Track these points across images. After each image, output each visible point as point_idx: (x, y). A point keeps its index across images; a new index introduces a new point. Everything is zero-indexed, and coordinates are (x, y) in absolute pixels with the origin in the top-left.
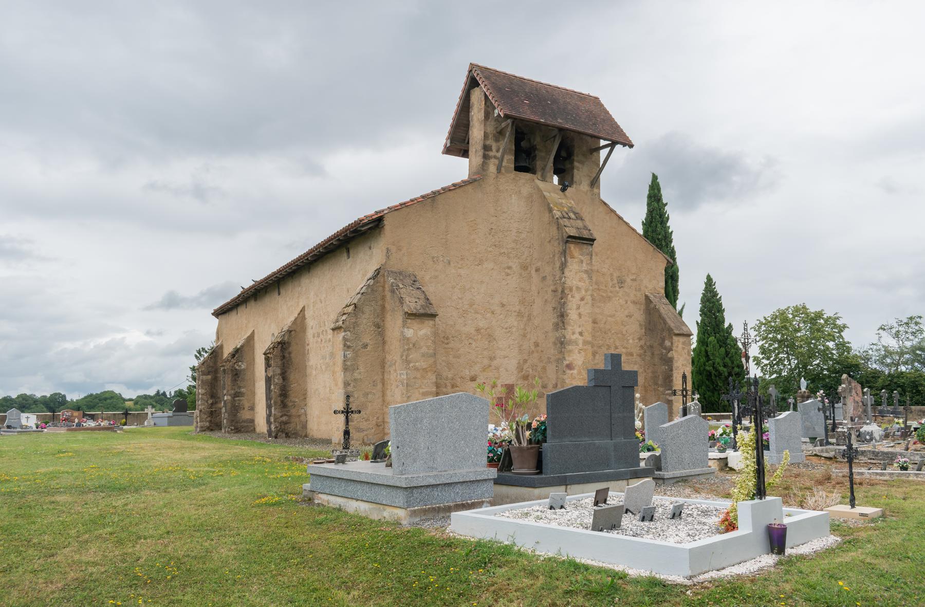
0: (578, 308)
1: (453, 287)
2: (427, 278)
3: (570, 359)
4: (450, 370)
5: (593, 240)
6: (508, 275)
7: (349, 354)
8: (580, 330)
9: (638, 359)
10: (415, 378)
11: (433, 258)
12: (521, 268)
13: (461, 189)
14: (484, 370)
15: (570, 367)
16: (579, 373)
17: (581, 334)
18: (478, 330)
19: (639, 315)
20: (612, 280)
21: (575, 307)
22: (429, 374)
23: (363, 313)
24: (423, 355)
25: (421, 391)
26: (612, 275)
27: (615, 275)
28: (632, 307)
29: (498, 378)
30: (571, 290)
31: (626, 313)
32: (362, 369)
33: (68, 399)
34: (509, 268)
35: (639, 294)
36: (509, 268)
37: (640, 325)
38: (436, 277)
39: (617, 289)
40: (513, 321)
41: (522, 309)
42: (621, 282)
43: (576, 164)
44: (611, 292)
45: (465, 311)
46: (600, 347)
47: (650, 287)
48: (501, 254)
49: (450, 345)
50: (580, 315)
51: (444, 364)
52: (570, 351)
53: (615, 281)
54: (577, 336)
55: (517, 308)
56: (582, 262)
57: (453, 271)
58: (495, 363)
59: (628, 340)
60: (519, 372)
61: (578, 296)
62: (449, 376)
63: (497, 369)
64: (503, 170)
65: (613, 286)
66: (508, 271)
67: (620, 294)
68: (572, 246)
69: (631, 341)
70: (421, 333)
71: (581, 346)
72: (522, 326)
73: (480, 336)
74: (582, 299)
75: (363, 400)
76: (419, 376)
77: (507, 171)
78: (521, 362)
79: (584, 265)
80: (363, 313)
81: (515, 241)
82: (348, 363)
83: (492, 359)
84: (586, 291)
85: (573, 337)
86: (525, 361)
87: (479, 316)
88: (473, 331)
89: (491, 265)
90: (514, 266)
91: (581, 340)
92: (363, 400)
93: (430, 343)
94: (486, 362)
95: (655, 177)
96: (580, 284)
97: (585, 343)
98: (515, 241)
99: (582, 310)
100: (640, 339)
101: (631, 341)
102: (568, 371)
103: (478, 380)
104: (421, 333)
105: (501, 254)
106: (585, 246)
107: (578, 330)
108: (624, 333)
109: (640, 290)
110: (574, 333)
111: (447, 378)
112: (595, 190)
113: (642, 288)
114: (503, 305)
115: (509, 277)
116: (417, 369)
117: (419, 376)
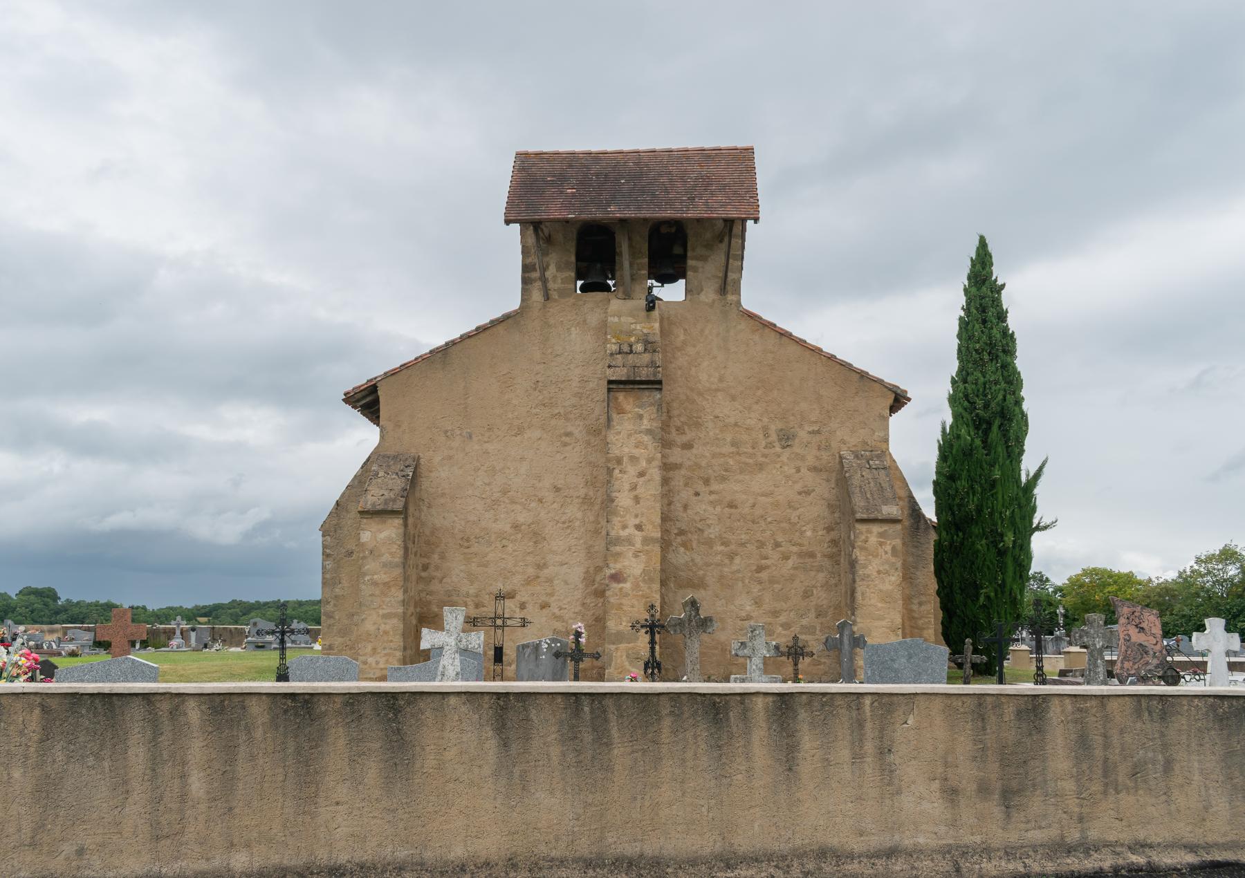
0: (634, 487)
1: (477, 470)
2: (437, 459)
3: (618, 566)
4: (472, 583)
5: (660, 382)
6: (565, 445)
7: (330, 564)
8: (637, 521)
9: (827, 563)
10: (371, 595)
11: (446, 432)
12: (588, 433)
13: (488, 332)
14: (528, 582)
15: (617, 578)
16: (636, 586)
17: (639, 527)
18: (516, 527)
19: (824, 489)
20: (766, 435)
21: (627, 486)
22: (393, 590)
23: (348, 512)
24: (384, 565)
25: (381, 612)
26: (765, 430)
27: (773, 427)
28: (809, 478)
29: (552, 595)
30: (619, 461)
31: (798, 487)
32: (345, 583)
33: (150, 608)
34: (568, 434)
35: (825, 455)
36: (568, 434)
37: (830, 506)
38: (450, 458)
39: (778, 449)
40: (573, 511)
41: (591, 493)
42: (786, 438)
43: (690, 263)
44: (765, 456)
45: (496, 502)
46: (743, 545)
47: (853, 441)
48: (553, 416)
49: (472, 550)
50: (637, 499)
51: (462, 575)
52: (619, 554)
53: (774, 437)
54: (631, 530)
55: (582, 492)
56: (641, 417)
57: (476, 447)
58: (546, 572)
59: (802, 533)
60: (587, 586)
61: (632, 471)
62: (471, 592)
63: (550, 580)
64: (555, 295)
65: (770, 445)
66: (567, 439)
67: (784, 458)
68: (621, 396)
69: (809, 533)
70: (383, 535)
71: (638, 545)
72: (592, 518)
73: (520, 536)
74: (641, 474)
75: (346, 622)
76: (377, 592)
77: (563, 293)
78: (591, 570)
79: (645, 421)
80: (348, 512)
81: (579, 395)
82: (328, 576)
83: (540, 567)
84: (649, 461)
85: (624, 533)
86: (599, 569)
87: (519, 507)
88: (508, 528)
89: (537, 433)
90: (576, 432)
91: (638, 537)
92: (346, 622)
93: (394, 548)
94: (531, 571)
95: (983, 244)
96: (636, 452)
97: (646, 541)
98: (579, 395)
99: (640, 491)
100: (829, 529)
101: (809, 533)
102: (614, 585)
103: (518, 597)
104: (383, 535)
105: (553, 416)
106: (647, 393)
107: (633, 521)
108: (794, 519)
109: (828, 447)
110: (624, 527)
111: (468, 595)
112: (730, 297)
113: (834, 444)
114: (557, 490)
115: (568, 448)
116: (375, 584)
117: (377, 592)
